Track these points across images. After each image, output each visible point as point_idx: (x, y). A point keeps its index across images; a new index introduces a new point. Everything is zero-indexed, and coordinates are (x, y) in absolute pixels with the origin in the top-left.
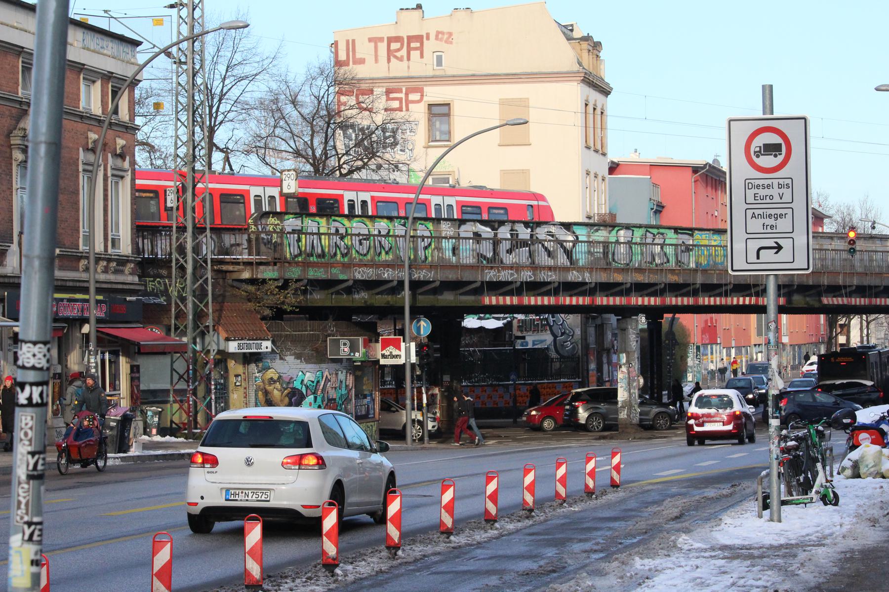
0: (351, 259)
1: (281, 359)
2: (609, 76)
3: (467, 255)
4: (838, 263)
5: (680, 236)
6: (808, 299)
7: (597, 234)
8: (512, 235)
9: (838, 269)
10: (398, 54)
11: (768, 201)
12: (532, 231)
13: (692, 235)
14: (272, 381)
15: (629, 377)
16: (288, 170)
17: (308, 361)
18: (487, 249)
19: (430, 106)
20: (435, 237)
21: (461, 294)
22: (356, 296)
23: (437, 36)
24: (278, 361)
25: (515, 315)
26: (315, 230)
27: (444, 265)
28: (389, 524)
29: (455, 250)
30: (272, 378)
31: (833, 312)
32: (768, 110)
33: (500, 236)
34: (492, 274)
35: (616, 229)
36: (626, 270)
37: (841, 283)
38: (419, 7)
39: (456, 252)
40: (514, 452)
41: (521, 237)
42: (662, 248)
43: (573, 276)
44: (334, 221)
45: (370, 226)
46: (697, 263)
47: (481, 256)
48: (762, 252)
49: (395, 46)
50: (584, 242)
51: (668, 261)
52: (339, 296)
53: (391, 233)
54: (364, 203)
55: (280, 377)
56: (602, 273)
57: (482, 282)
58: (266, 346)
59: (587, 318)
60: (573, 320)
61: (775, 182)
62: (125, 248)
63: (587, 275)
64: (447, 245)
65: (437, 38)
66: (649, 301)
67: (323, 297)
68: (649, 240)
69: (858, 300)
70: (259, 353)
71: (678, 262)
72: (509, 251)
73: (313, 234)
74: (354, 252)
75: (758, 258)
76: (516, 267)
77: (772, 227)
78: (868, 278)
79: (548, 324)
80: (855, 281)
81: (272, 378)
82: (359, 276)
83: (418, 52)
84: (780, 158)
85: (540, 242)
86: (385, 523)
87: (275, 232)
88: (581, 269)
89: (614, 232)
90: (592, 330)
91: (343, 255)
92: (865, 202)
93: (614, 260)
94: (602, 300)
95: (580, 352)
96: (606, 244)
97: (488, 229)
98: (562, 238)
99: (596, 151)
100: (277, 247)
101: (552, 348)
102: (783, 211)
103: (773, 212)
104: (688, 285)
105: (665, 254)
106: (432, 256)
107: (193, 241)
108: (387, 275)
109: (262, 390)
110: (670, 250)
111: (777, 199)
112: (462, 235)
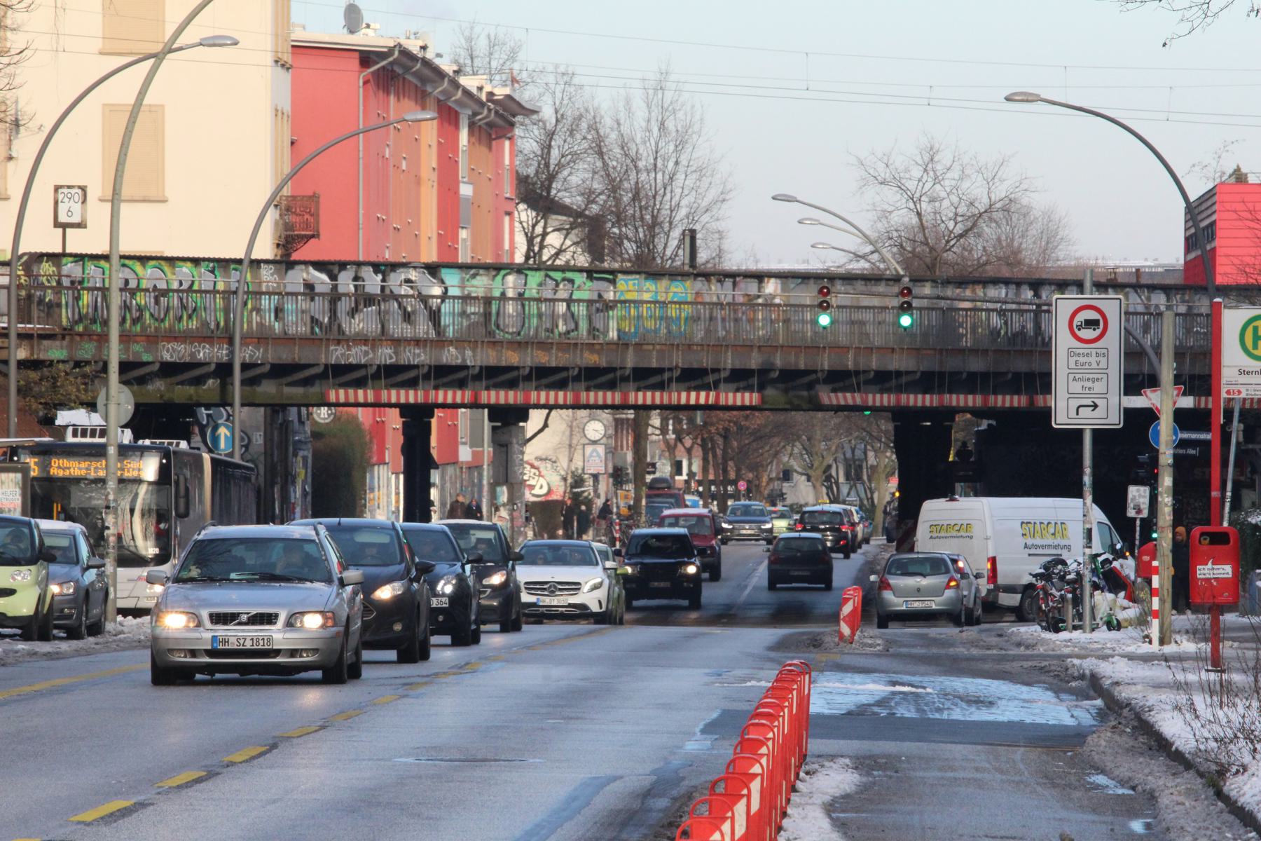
0: (144, 328)
7: (474, 282)
9: (843, 340)
12: (384, 280)
13: (613, 282)
16: (69, 187)
18: (319, 309)
20: (253, 293)
21: (289, 384)
22: (150, 387)
27: (261, 338)
28: (843, 624)
29: (278, 311)
34: (339, 353)
35: (503, 272)
39: (280, 315)
40: (40, 694)
41: (369, 289)
42: (568, 307)
43: (450, 356)
45: (170, 276)
46: (619, 330)
50: (458, 298)
51: (577, 328)
53: (196, 287)
57: (326, 366)
61: (1094, 352)
63: (469, 353)
68: (549, 295)
69: (920, 397)
71: (592, 330)
72: (353, 312)
74: (147, 315)
76: (362, 339)
80: (875, 363)
82: (167, 357)
84: (1098, 332)
85: (396, 298)
86: (838, 622)
88: (458, 342)
89: (499, 278)
93: (498, 327)
96: (488, 301)
97: (324, 277)
102: (1099, 376)
103: (1091, 376)
104: (613, 370)
105: (573, 315)
110: (581, 310)
111: (1094, 365)
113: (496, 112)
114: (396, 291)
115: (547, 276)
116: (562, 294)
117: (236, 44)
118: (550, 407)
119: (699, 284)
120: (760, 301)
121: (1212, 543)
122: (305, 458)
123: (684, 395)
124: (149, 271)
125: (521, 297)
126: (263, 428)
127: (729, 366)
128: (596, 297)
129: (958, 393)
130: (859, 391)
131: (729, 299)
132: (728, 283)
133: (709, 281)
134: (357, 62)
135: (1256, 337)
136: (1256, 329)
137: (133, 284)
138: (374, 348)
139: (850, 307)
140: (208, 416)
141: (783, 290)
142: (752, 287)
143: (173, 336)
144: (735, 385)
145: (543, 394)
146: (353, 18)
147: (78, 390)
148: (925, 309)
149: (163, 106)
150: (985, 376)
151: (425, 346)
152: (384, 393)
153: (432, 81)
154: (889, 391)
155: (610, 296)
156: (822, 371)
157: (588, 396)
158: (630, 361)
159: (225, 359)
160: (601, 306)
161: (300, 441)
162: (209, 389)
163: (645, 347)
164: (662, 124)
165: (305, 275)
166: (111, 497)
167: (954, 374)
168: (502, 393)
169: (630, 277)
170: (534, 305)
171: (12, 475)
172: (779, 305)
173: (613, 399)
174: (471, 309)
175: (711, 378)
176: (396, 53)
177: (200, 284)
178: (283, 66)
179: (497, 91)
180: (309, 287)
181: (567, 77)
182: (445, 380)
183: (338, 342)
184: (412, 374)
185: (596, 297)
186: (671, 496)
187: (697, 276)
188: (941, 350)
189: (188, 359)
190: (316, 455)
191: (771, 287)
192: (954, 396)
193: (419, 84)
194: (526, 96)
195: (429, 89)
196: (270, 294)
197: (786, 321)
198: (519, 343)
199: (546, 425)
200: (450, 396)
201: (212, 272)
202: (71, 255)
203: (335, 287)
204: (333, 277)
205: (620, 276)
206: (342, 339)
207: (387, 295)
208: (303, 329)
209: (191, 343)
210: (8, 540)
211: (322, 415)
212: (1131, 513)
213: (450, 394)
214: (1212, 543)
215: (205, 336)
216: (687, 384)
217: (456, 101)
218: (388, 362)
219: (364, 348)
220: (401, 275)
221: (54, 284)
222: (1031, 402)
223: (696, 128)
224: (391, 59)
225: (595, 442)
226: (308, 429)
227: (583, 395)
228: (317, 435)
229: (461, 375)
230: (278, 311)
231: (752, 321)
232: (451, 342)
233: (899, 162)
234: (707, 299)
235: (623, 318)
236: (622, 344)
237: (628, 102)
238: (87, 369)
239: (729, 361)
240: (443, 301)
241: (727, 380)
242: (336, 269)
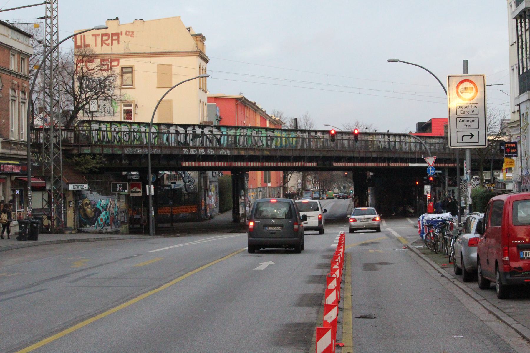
2: (208, 53)
8: (193, 132)
10: (107, 42)
11: (467, 114)
17: (102, 195)
18: (182, 139)
19: (122, 68)
23: (126, 33)
25: (165, 172)
26: (105, 129)
29: (168, 139)
31: (286, 170)
32: (466, 72)
33: (188, 132)
38: (117, 19)
41: (197, 132)
43: (221, 152)
47: (179, 142)
48: (464, 137)
49: (105, 38)
55: (90, 202)
59: (201, 174)
60: (194, 175)
62: (24, 139)
63: (228, 151)
64: (164, 137)
65: (126, 34)
73: (104, 131)
75: (462, 140)
77: (469, 126)
79: (181, 176)
82: (126, 152)
83: (117, 41)
85: (206, 135)
87: (87, 130)
90: (202, 180)
91: (118, 142)
92: (306, 116)
94: (205, 164)
97: (183, 129)
98: (215, 133)
99: (203, 91)
101: (184, 188)
102: (474, 119)
103: (469, 119)
108: (139, 151)
111: (471, 113)
112: (171, 131)
122: (216, 186)
150: (377, 158)
167: (369, 158)
191: (319, 134)
201: (145, 127)
202: (94, 121)
208: (174, 144)
212: (425, 194)
222: (389, 165)
232: (223, 148)
233: (351, 125)
236: (276, 149)
240: (221, 136)
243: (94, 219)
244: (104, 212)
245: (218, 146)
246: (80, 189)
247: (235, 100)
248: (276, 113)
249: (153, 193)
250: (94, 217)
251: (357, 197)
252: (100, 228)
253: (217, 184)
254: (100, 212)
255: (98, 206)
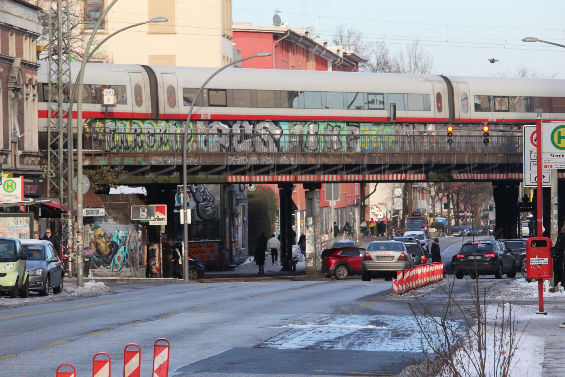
1: (106, 221)
3: (213, 147)
4: (463, 146)
5: (351, 128)
6: (440, 175)
9: (464, 151)
12: (254, 128)
13: (358, 127)
14: (100, 236)
15: (315, 235)
17: (121, 223)
20: (194, 134)
22: (147, 177)
24: (104, 222)
27: (197, 154)
29: (206, 142)
30: (100, 235)
34: (232, 160)
35: (308, 123)
36: (315, 155)
37: (466, 162)
39: (207, 143)
41: (247, 132)
43: (284, 160)
44: (134, 123)
45: (155, 127)
46: (361, 148)
50: (287, 135)
52: (137, 177)
53: (167, 132)
54: (42, 114)
55: (105, 234)
56: (302, 158)
57: (227, 166)
58: (102, 212)
63: (292, 159)
64: (202, 139)
66: (500, 176)
67: (128, 177)
68: (329, 133)
69: (498, 175)
70: (92, 217)
71: (349, 148)
72: (240, 142)
76: (244, 154)
78: (487, 158)
80: (477, 161)
81: (100, 235)
82: (153, 163)
85: (260, 135)
88: (287, 154)
89: (306, 126)
90: (226, 196)
93: (305, 147)
95: (219, 216)
96: (301, 136)
97: (226, 127)
100: (101, 143)
104: (358, 165)
106: (192, 147)
107: (64, 140)
108: (170, 161)
109: (94, 243)
113: (344, 60)
114: (259, 132)
115: (328, 124)
116: (335, 132)
117: (167, 21)
118: (377, 182)
119: (398, 127)
120: (425, 134)
121: (537, 246)
122: (244, 207)
123: (391, 176)
124: (146, 125)
125: (316, 134)
126: (219, 194)
127: (411, 163)
128: (350, 133)
129: (515, 173)
130: (470, 172)
131: (411, 133)
132: (411, 126)
133: (402, 125)
134: (272, 37)
135: (560, 137)
136: (559, 133)
137: (139, 131)
138: (248, 157)
139: (466, 136)
140: (196, 189)
141: (436, 129)
142: (421, 128)
143: (157, 154)
144: (414, 171)
145: (326, 176)
146: (277, 20)
147: (113, 178)
148: (500, 136)
149: (175, 56)
151: (272, 156)
152: (254, 177)
153: (311, 47)
154: (483, 172)
155: (357, 133)
156: (454, 164)
157: (347, 177)
158: (366, 161)
159: (180, 163)
160: (354, 138)
161: (240, 199)
162: (174, 177)
163: (373, 155)
164: (416, 64)
165: (217, 126)
166: (80, 227)
168: (308, 176)
169: (366, 124)
170: (322, 137)
171: (25, 218)
172: (433, 136)
173: (359, 178)
174: (293, 140)
175: (403, 168)
176: (288, 34)
177: (169, 131)
178: (227, 38)
179: (347, 52)
180: (220, 131)
181: (382, 46)
182: (282, 171)
183: (232, 155)
184: (266, 169)
185: (350, 133)
186: (422, 219)
187: (396, 123)
188: (507, 154)
189: (163, 164)
190: (250, 205)
192: (514, 174)
193: (305, 48)
194: (361, 55)
195: (310, 50)
196: (201, 134)
197: (437, 143)
198: (315, 154)
199: (375, 190)
200: (331, 177)
201: (175, 125)
203: (231, 131)
204: (230, 127)
205: (361, 124)
206: (235, 153)
207: (255, 134)
208: (216, 150)
209: (165, 157)
210: (6, 250)
211: (253, 188)
213: (284, 177)
214: (537, 246)
215: (171, 154)
216: (393, 171)
217: (324, 55)
218: (255, 163)
219: (244, 158)
220: (262, 125)
221: (102, 131)
223: (430, 65)
224: (286, 36)
225: (398, 197)
226: (245, 193)
227: (345, 177)
228: (250, 196)
229: (289, 169)
230: (206, 142)
231: (422, 143)
232: (284, 154)
234: (401, 134)
235: (362, 143)
236: (362, 154)
237: (401, 55)
238: (117, 169)
239: (411, 161)
241: (410, 169)
242: (231, 123)
243: (110, 257)
244: (122, 248)
245: (276, 149)
246: (95, 215)
247: (271, 36)
248: (346, 34)
249: (189, 221)
250: (109, 255)
251: (501, 230)
252: (116, 270)
253: (246, 205)
254: (117, 248)
255: (114, 239)
